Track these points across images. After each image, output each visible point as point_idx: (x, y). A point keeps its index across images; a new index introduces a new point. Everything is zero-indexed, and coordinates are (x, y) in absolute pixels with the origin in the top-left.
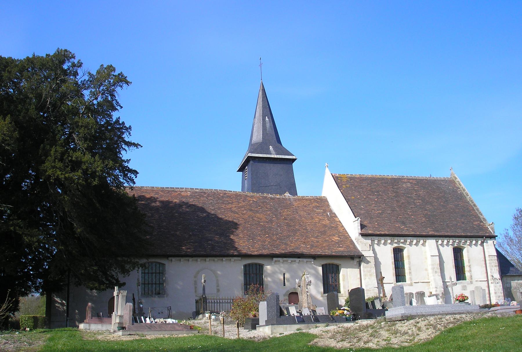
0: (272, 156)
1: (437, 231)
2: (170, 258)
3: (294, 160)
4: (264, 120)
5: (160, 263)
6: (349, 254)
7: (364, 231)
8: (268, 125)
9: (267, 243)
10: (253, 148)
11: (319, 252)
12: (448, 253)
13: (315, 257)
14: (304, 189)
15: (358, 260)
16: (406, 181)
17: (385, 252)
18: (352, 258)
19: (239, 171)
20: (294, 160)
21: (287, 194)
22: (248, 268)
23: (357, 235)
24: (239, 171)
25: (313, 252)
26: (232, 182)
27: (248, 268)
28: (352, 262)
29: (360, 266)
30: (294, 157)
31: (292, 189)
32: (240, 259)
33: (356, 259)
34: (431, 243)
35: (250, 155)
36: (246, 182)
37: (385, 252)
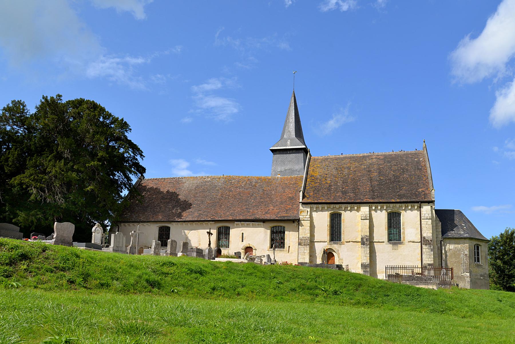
1: (373, 198)
11: (268, 217)
12: (381, 217)
13: (264, 221)
18: (293, 221)
32: (213, 223)
34: (365, 210)
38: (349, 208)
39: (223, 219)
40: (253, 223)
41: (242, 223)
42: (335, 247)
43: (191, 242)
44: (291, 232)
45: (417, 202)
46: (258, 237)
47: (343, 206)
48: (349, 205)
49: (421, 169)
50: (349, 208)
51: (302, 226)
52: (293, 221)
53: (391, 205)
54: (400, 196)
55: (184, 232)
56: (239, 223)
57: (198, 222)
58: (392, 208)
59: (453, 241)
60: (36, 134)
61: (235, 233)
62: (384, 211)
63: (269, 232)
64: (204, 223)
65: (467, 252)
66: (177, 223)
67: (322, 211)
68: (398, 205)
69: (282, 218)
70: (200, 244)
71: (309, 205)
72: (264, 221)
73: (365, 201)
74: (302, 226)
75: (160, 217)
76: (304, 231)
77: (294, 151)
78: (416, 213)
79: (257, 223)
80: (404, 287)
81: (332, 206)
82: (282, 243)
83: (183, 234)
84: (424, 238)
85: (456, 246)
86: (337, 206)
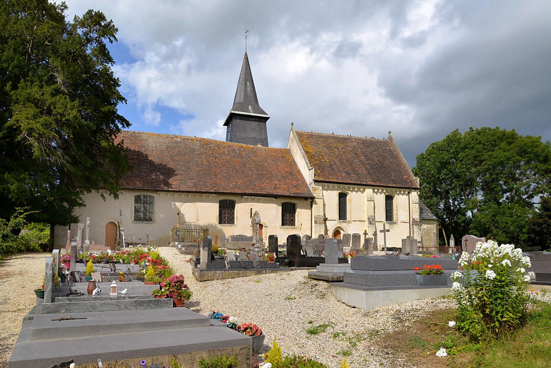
0: (251, 114)
1: (375, 182)
2: (158, 193)
3: (268, 118)
4: (246, 84)
5: (150, 196)
6: (304, 195)
7: (317, 178)
8: (249, 89)
9: (239, 183)
10: (236, 106)
11: (280, 192)
12: (380, 199)
13: (276, 197)
14: (274, 144)
15: (311, 201)
16: (353, 140)
17: (330, 197)
18: (306, 199)
19: (224, 125)
20: (268, 118)
21: (260, 146)
22: (222, 203)
23: (311, 181)
24: (224, 125)
25: (275, 192)
26: (218, 132)
27: (222, 203)
28: (306, 202)
29: (312, 207)
30: (267, 116)
31: (265, 142)
32: (216, 195)
33: (310, 200)
34: (369, 191)
35: (232, 112)
36: (229, 134)
37: (330, 197)
38: (356, 190)
39: (229, 191)
40: (265, 198)
41: (252, 197)
42: (343, 225)
43: (185, 217)
44: (303, 210)
45: (409, 188)
46: (270, 213)
47: (352, 186)
48: (356, 186)
49: (395, 158)
50: (356, 190)
51: (316, 204)
52: (306, 199)
53: (389, 189)
54: (394, 182)
55: (175, 205)
56: (249, 197)
57: (197, 194)
58: (390, 191)
59: (426, 222)
60: (60, 11)
61: (242, 209)
62: (383, 194)
63: (217, 205)
64: (197, 195)
65: (435, 232)
66: (165, 193)
67: (332, 190)
68: (394, 189)
69: (296, 195)
70: (198, 220)
71: (321, 184)
72: (276, 197)
73: (369, 183)
74: (316, 204)
75: (139, 185)
76: (317, 209)
77: (256, 119)
78: (406, 197)
79: (270, 199)
80: (171, 244)
81: (342, 186)
82: (292, 220)
83: (173, 206)
84: (414, 219)
85: (428, 226)
86: (346, 186)
